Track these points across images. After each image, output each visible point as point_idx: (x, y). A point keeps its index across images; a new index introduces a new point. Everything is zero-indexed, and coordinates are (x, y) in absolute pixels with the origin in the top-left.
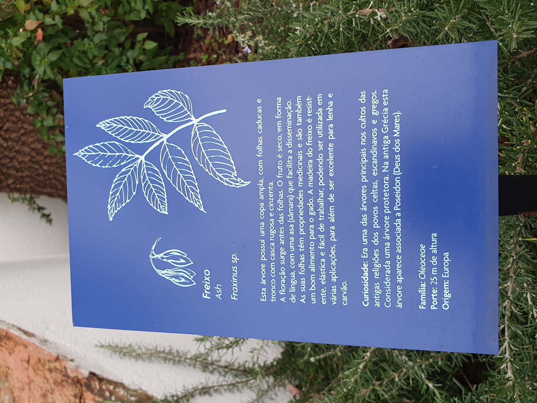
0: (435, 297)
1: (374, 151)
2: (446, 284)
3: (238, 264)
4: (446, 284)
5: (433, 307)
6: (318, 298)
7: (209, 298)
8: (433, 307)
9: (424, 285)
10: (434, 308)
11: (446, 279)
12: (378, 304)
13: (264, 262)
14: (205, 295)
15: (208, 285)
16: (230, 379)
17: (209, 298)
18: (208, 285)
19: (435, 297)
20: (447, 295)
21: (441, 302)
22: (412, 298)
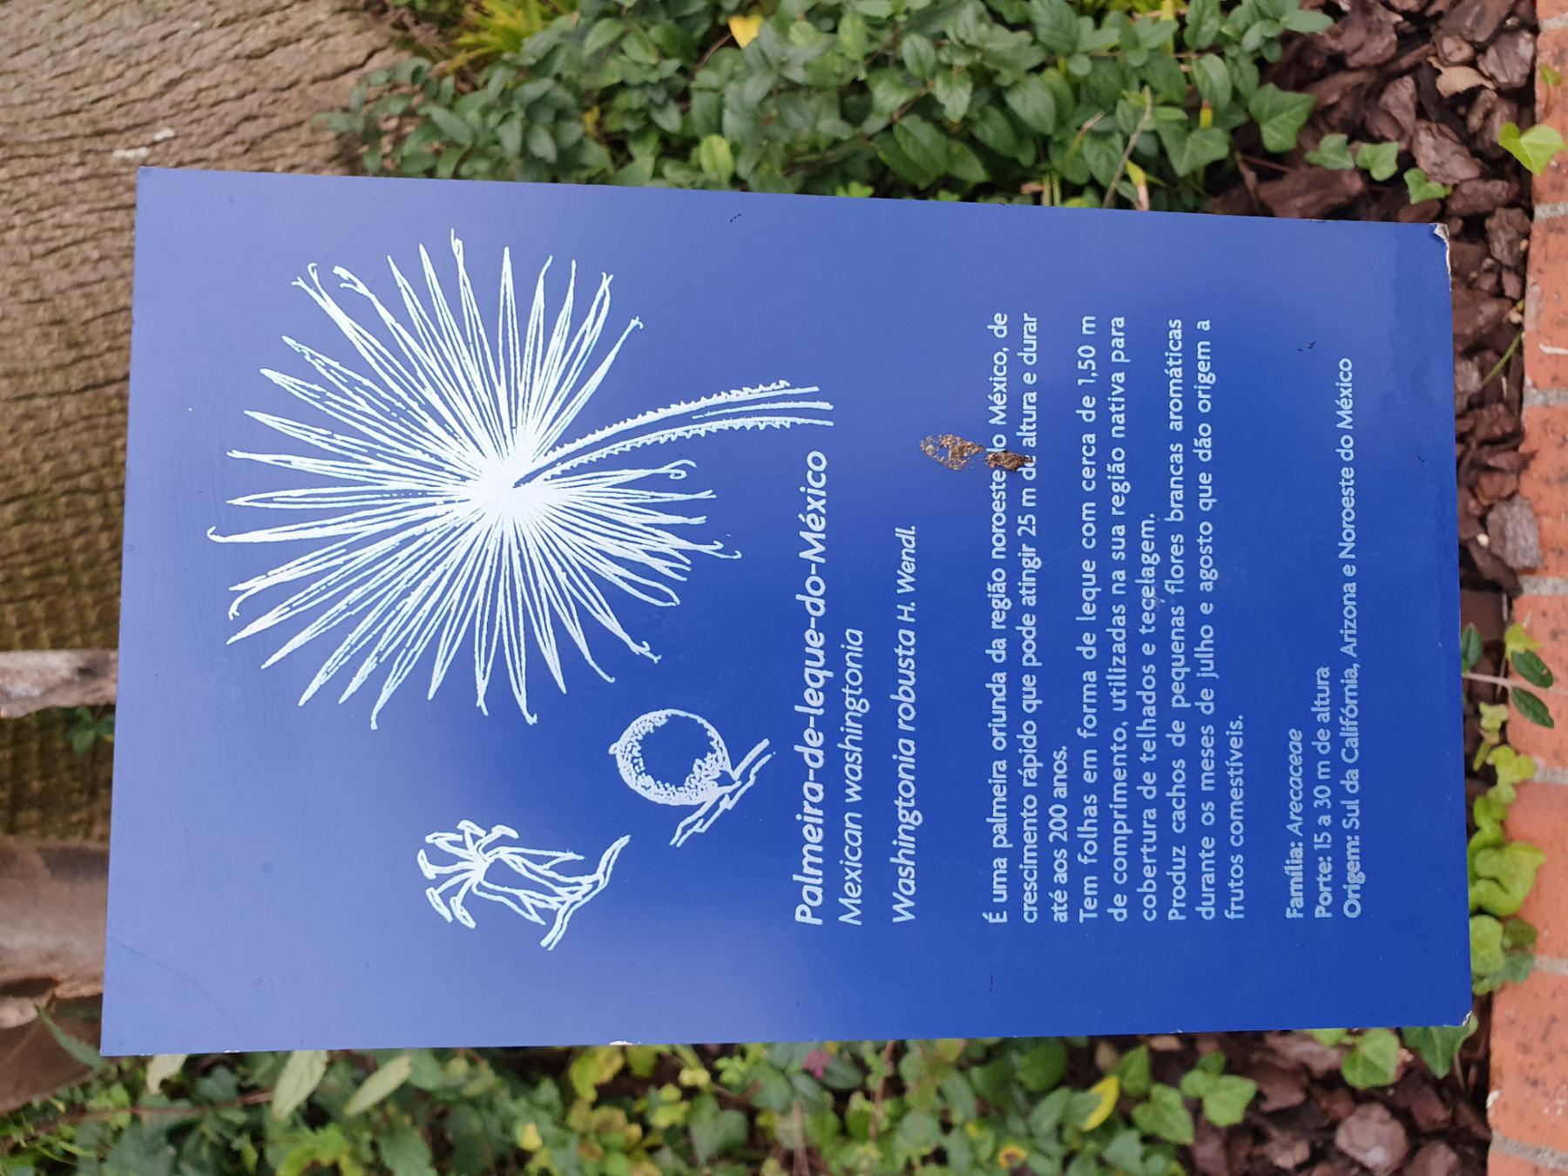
0: (1326, 884)
1: (1179, 668)
2: (1353, 844)
3: (1038, 575)
4: (1353, 844)
5: (1173, 915)
6: (1075, 903)
7: (819, 922)
8: (1320, 912)
9: (1297, 852)
10: (809, 919)
11: (1352, 832)
12: (1061, 916)
13: (1002, 853)
14: (803, 914)
15: (816, 826)
16: (1393, 67)
17: (819, 922)
18: (816, 826)
19: (1326, 884)
20: (1356, 877)
21: (1339, 896)
22: (1267, 888)
